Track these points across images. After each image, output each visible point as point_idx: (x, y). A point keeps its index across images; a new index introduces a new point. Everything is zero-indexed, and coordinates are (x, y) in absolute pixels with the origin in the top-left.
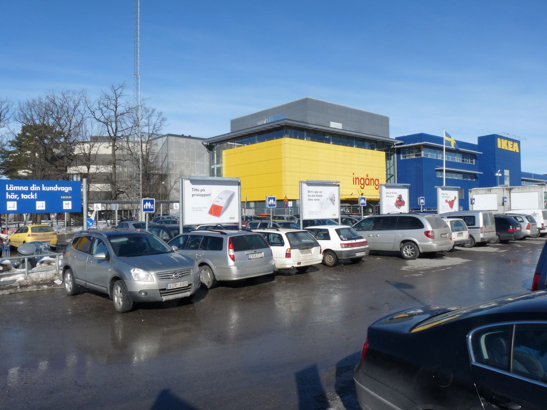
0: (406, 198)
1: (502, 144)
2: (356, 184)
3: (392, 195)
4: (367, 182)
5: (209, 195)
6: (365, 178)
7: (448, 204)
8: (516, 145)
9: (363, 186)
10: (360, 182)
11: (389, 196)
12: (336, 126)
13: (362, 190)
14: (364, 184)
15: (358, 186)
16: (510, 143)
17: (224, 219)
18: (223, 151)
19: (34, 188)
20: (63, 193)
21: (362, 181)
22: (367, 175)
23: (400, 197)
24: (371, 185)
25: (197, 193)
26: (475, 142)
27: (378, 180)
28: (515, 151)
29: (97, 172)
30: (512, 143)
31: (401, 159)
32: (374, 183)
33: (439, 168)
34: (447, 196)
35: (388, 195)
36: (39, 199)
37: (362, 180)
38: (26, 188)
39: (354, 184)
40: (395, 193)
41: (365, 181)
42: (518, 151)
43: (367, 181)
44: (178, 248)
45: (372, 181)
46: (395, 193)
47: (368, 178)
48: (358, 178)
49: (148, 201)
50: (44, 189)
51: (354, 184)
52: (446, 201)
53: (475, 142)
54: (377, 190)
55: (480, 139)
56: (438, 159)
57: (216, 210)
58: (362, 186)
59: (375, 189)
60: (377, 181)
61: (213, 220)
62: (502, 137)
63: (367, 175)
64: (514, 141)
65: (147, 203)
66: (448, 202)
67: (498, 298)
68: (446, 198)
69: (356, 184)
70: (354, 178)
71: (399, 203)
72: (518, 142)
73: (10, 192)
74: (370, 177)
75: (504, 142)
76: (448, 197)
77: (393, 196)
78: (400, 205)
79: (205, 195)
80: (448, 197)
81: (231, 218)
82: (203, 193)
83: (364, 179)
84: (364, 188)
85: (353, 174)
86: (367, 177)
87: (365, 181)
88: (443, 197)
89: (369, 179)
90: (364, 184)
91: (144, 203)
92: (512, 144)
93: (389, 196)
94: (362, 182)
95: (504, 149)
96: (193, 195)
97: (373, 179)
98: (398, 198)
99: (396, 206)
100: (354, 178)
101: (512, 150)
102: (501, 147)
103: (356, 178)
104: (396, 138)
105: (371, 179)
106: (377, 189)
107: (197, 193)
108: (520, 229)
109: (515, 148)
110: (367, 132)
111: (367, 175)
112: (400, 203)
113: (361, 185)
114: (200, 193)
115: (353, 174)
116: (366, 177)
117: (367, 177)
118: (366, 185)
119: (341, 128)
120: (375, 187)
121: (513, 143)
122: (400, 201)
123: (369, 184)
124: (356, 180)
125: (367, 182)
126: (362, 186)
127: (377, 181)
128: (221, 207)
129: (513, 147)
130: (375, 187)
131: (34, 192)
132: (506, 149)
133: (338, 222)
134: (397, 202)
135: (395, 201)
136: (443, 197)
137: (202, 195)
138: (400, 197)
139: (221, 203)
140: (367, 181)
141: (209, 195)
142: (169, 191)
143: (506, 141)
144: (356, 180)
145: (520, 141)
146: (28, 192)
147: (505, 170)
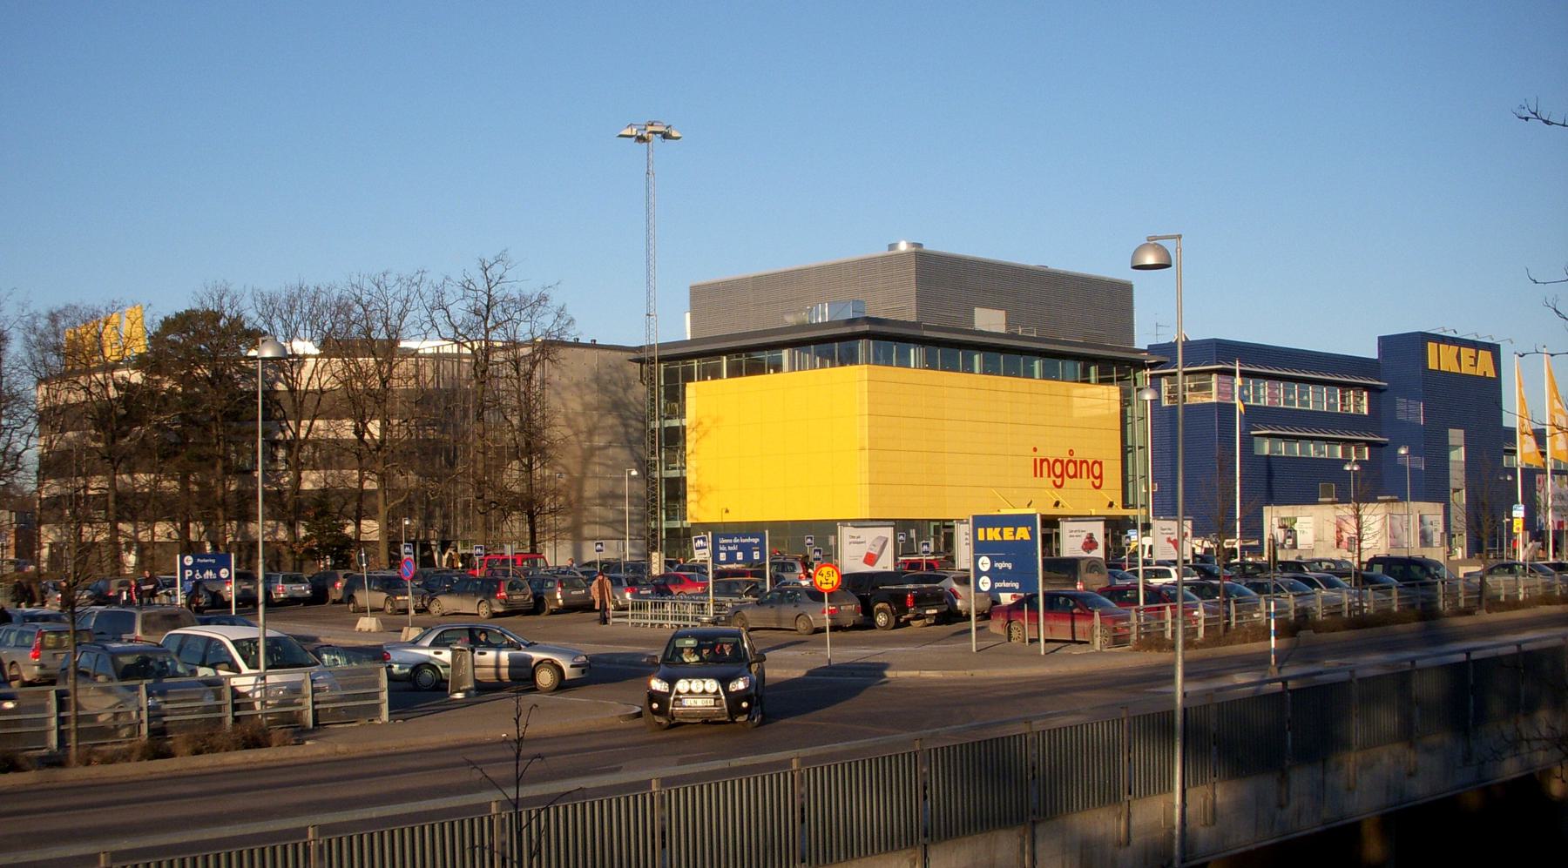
0: (1100, 538)
2: (1041, 476)
7: (1171, 545)
8: (1485, 356)
9: (1060, 479)
10: (1051, 469)
15: (1047, 481)
16: (1466, 353)
19: (736, 540)
21: (1058, 470)
22: (1071, 452)
23: (1090, 537)
24: (1081, 477)
26: (1371, 352)
28: (1482, 374)
30: (1472, 352)
34: (1169, 532)
36: (739, 551)
39: (1036, 476)
41: (1065, 468)
42: (1491, 374)
44: (253, 703)
45: (1084, 465)
49: (700, 539)
51: (1036, 476)
52: (1169, 540)
53: (1371, 352)
54: (1095, 490)
56: (1262, 403)
57: (870, 559)
58: (1059, 481)
59: (1091, 487)
61: (867, 569)
62: (1441, 339)
63: (1071, 452)
64: (1476, 345)
66: (1171, 542)
68: (1168, 536)
69: (1041, 476)
70: (1035, 460)
71: (1089, 545)
72: (1494, 349)
74: (1077, 457)
75: (1448, 352)
82: (859, 540)
83: (1062, 462)
85: (1035, 450)
86: (1072, 455)
87: (1065, 468)
89: (1076, 461)
90: (1061, 476)
91: (696, 542)
95: (1448, 370)
96: (850, 543)
97: (1086, 462)
100: (1035, 460)
103: (1042, 461)
104: (1149, 346)
105: (1082, 462)
106: (1098, 488)
109: (1485, 366)
110: (1071, 337)
111: (1071, 450)
112: (1090, 544)
115: (1035, 450)
117: (1072, 455)
119: (1002, 330)
120: (1093, 483)
122: (1091, 542)
123: (1075, 476)
124: (1042, 466)
126: (1059, 483)
127: (1097, 467)
129: (1476, 365)
130: (1093, 483)
131: (736, 544)
132: (1455, 369)
133: (1530, 569)
134: (1085, 543)
138: (1090, 537)
139: (875, 551)
143: (1454, 349)
144: (1042, 466)
146: (731, 545)
147: (1450, 430)
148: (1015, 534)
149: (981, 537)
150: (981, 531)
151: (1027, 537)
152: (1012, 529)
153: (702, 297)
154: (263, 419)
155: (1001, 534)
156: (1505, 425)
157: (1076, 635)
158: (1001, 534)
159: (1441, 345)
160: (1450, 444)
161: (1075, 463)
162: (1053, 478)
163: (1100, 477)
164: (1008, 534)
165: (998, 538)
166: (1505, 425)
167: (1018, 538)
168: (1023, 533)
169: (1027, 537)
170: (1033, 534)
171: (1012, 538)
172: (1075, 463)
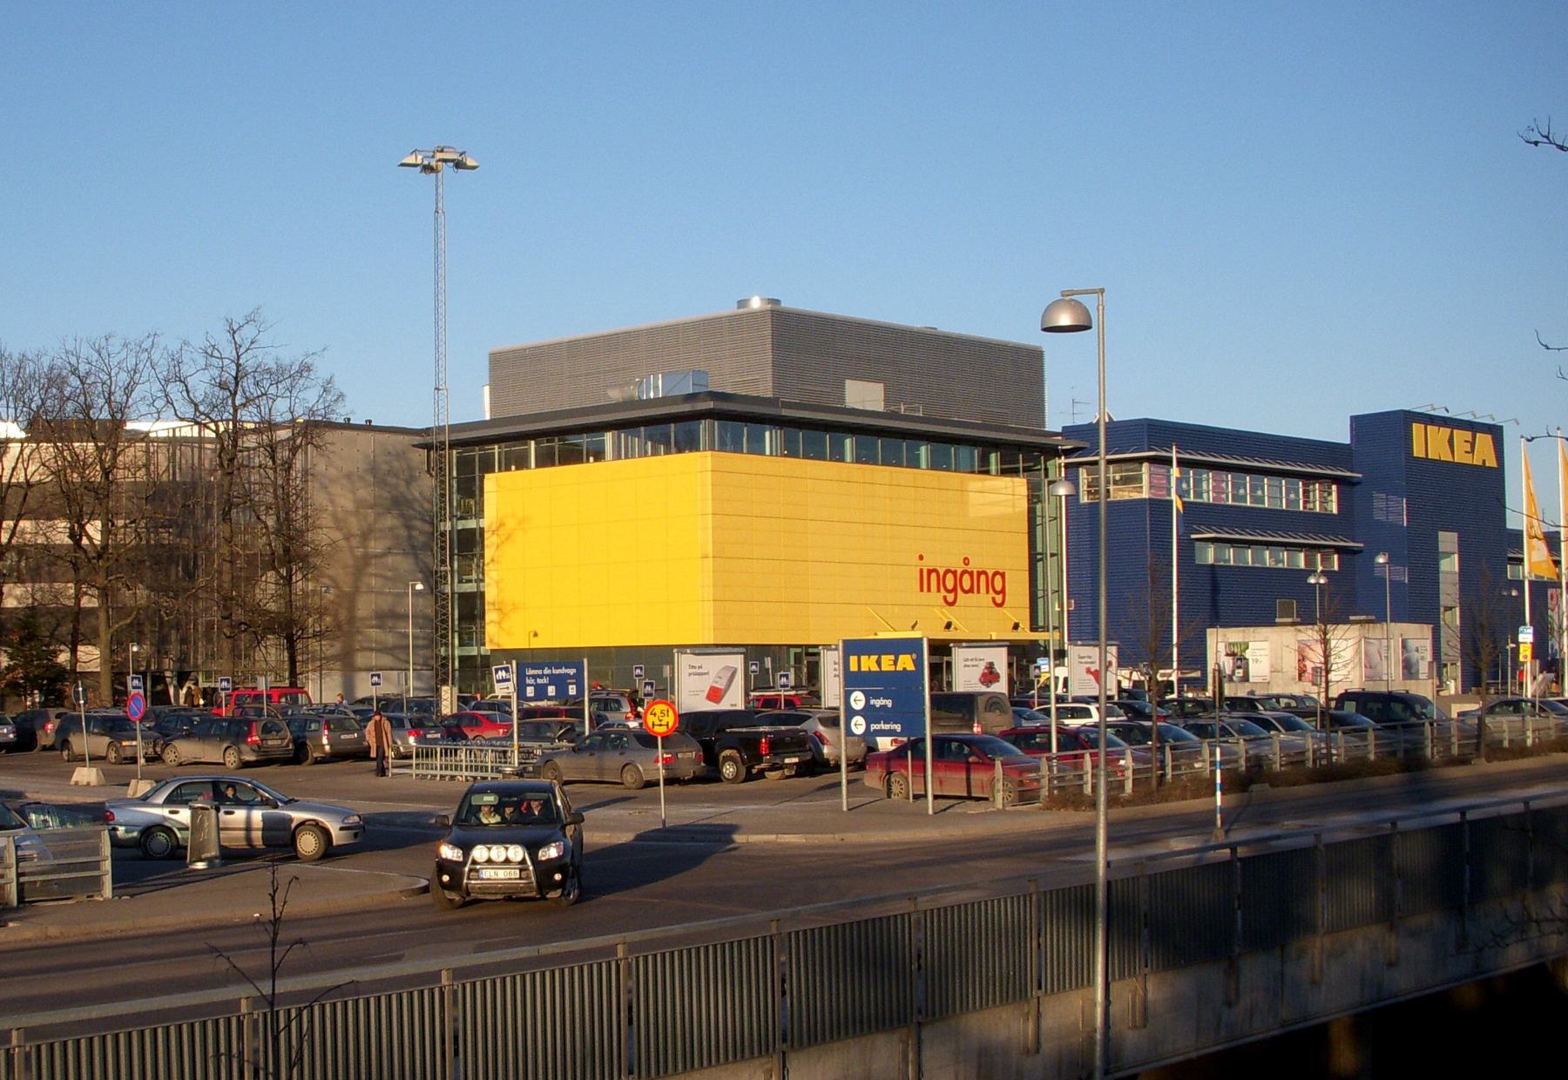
0: (1002, 668)
1: (1429, 444)
2: (929, 590)
3: (976, 663)
4: (966, 584)
5: (708, 673)
8: (1484, 441)
10: (941, 581)
12: (864, 396)
13: (946, 610)
14: (954, 590)
15: (936, 597)
16: (1461, 436)
18: (487, 476)
19: (547, 671)
20: (568, 676)
21: (950, 583)
22: (966, 561)
23: (990, 666)
24: (979, 592)
25: (694, 670)
26: (1343, 436)
27: (1003, 575)
28: (1480, 463)
30: (1468, 435)
31: (1081, 502)
34: (1089, 660)
35: (968, 663)
37: (950, 577)
38: (540, 672)
39: (922, 590)
40: (981, 660)
42: (1492, 462)
46: (981, 660)
48: (935, 571)
49: (501, 669)
51: (922, 590)
52: (1088, 671)
53: (1343, 436)
55: (1360, 424)
58: (950, 597)
61: (711, 707)
63: (966, 561)
64: (1473, 427)
68: (1088, 666)
70: (921, 571)
71: (989, 677)
72: (1495, 432)
73: (529, 676)
74: (974, 566)
75: (1438, 435)
76: (1092, 663)
77: (976, 666)
78: (991, 682)
79: (699, 674)
80: (1092, 663)
82: (700, 671)
83: (954, 573)
85: (921, 558)
90: (954, 590)
92: (1470, 439)
94: (950, 585)
96: (690, 674)
98: (986, 668)
99: (982, 683)
100: (921, 571)
104: (1064, 428)
105: (979, 574)
107: (694, 670)
109: (1483, 452)
110: (966, 416)
111: (966, 559)
112: (990, 676)
115: (921, 558)
116: (962, 565)
122: (991, 673)
123: (971, 590)
124: (929, 578)
125: (966, 584)
128: (720, 689)
131: (547, 675)
132: (1446, 457)
133: (1540, 707)
134: (984, 675)
137: (699, 674)
138: (990, 666)
139: (721, 685)
141: (708, 673)
143: (1445, 432)
144: (929, 578)
145: (1500, 428)
146: (541, 676)
148: (895, 663)
149: (853, 667)
150: (853, 659)
151: (911, 667)
152: (892, 657)
155: (879, 663)
156: (1456, 534)
158: (879, 663)
159: (1429, 427)
161: (971, 574)
163: (1003, 592)
164: (887, 663)
165: (875, 668)
167: (899, 668)
168: (906, 662)
169: (911, 667)
170: (918, 663)
172: (971, 574)
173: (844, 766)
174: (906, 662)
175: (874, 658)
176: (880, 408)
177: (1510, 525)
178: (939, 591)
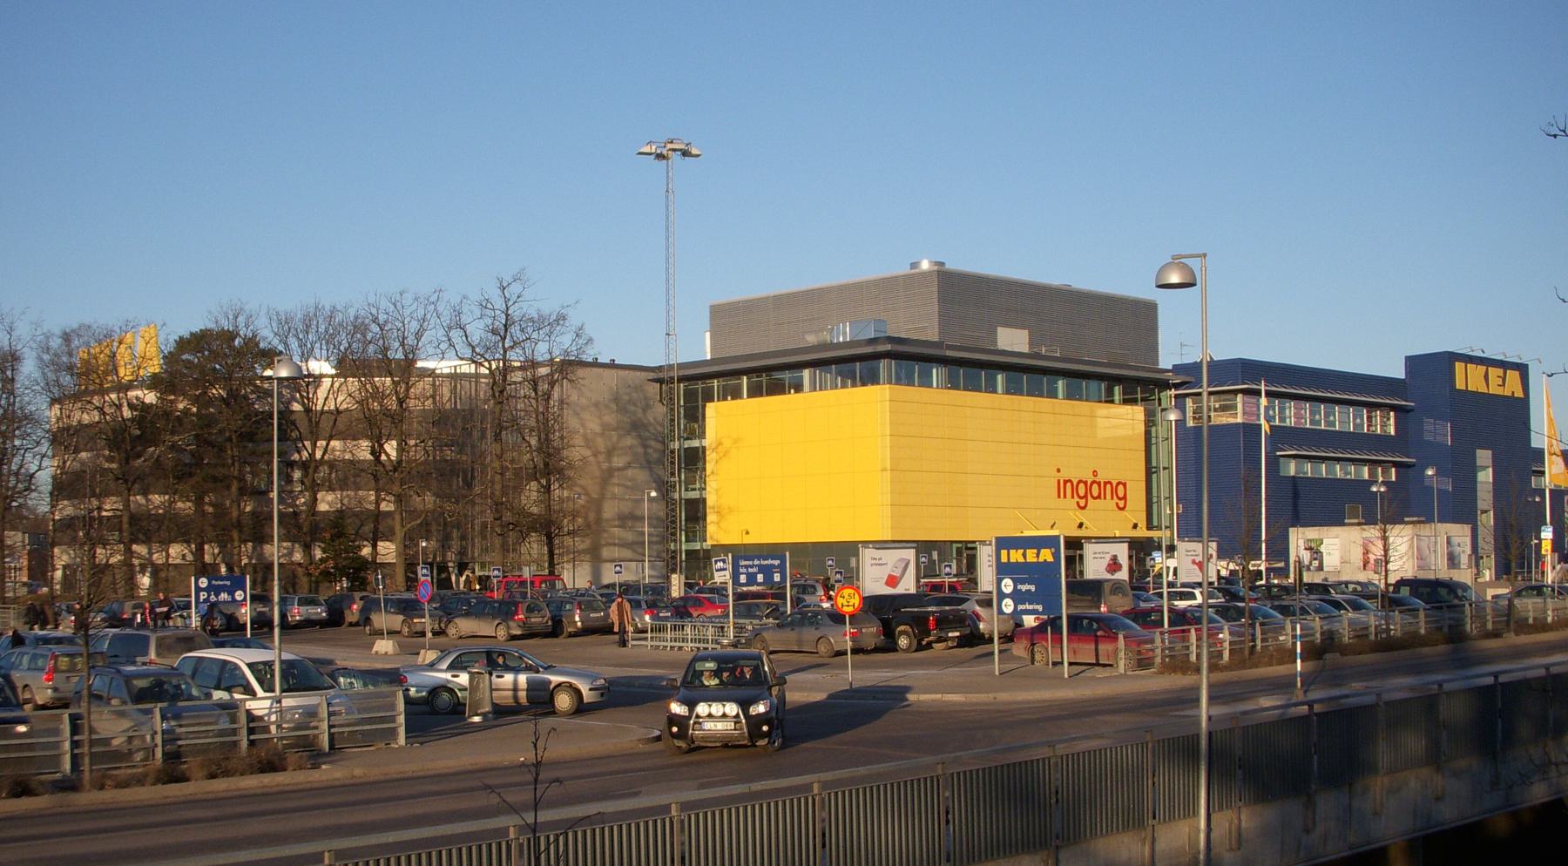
1: (1469, 379)
2: (1065, 497)
6: (1090, 479)
7: (1196, 567)
8: (1513, 376)
9: (1084, 500)
10: (1075, 490)
11: (1096, 558)
15: (1071, 502)
16: (1494, 372)
17: (900, 590)
18: (708, 404)
19: (756, 562)
20: (773, 566)
21: (1082, 491)
22: (1095, 473)
23: (1115, 558)
24: (1105, 498)
26: (1399, 373)
27: (1125, 485)
29: (326, 457)
30: (1500, 372)
32: (1114, 492)
33: (1286, 451)
34: (1194, 553)
37: (1082, 486)
38: (751, 563)
39: (1059, 497)
41: (1088, 488)
42: (1519, 394)
43: (1095, 487)
45: (1108, 486)
47: (1097, 479)
48: (1070, 481)
49: (720, 561)
50: (762, 562)
51: (1059, 497)
54: (1121, 512)
55: (1412, 362)
58: (1082, 503)
59: (1116, 509)
60: (1121, 488)
63: (1095, 473)
64: (1504, 365)
65: (718, 563)
67: (1485, 813)
69: (1065, 497)
70: (1059, 481)
72: (1522, 369)
73: (742, 566)
74: (1101, 478)
75: (1476, 372)
78: (1115, 571)
80: (1197, 555)
81: (906, 590)
82: (880, 562)
83: (1085, 483)
84: (1088, 508)
85: (1059, 471)
86: (1095, 476)
87: (1088, 488)
88: (1188, 555)
90: (1085, 497)
91: (716, 563)
93: (1096, 558)
95: (1476, 390)
97: (1111, 483)
98: (1111, 560)
100: (1059, 481)
101: (1502, 394)
102: (1467, 387)
104: (1174, 366)
105: (1106, 483)
108: (759, 581)
109: (1513, 386)
110: (1095, 356)
111: (1095, 471)
112: (1114, 566)
113: (1079, 500)
114: (878, 562)
115: (1059, 471)
116: (1092, 477)
117: (1095, 476)
118: (1093, 500)
120: (1117, 504)
121: (1505, 373)
122: (1115, 563)
123: (1099, 497)
124: (1065, 487)
127: (1121, 488)
130: (1117, 504)
132: (1483, 389)
134: (1109, 565)
135: (1105, 566)
136: (1188, 555)
138: (1115, 558)
139: (897, 573)
140: (1095, 487)
142: (1284, 633)
143: (1482, 369)
144: (1065, 487)
146: (752, 567)
149: (1004, 559)
150: (1004, 553)
151: (1050, 559)
152: (1035, 551)
153: (723, 316)
154: (279, 440)
155: (1024, 555)
156: (1533, 445)
157: (1100, 658)
158: (1024, 555)
160: (1478, 464)
161: (1099, 484)
162: (1076, 499)
163: (1124, 498)
164: (1031, 555)
165: (1021, 560)
166: (1533, 445)
167: (1041, 560)
168: (1046, 555)
169: (1050, 559)
170: (1056, 555)
171: (1035, 560)
172: (1099, 484)
173: (996, 639)
174: (1046, 555)
175: (1021, 551)
176: (1025, 349)
177: (1534, 445)
178: (1073, 497)
